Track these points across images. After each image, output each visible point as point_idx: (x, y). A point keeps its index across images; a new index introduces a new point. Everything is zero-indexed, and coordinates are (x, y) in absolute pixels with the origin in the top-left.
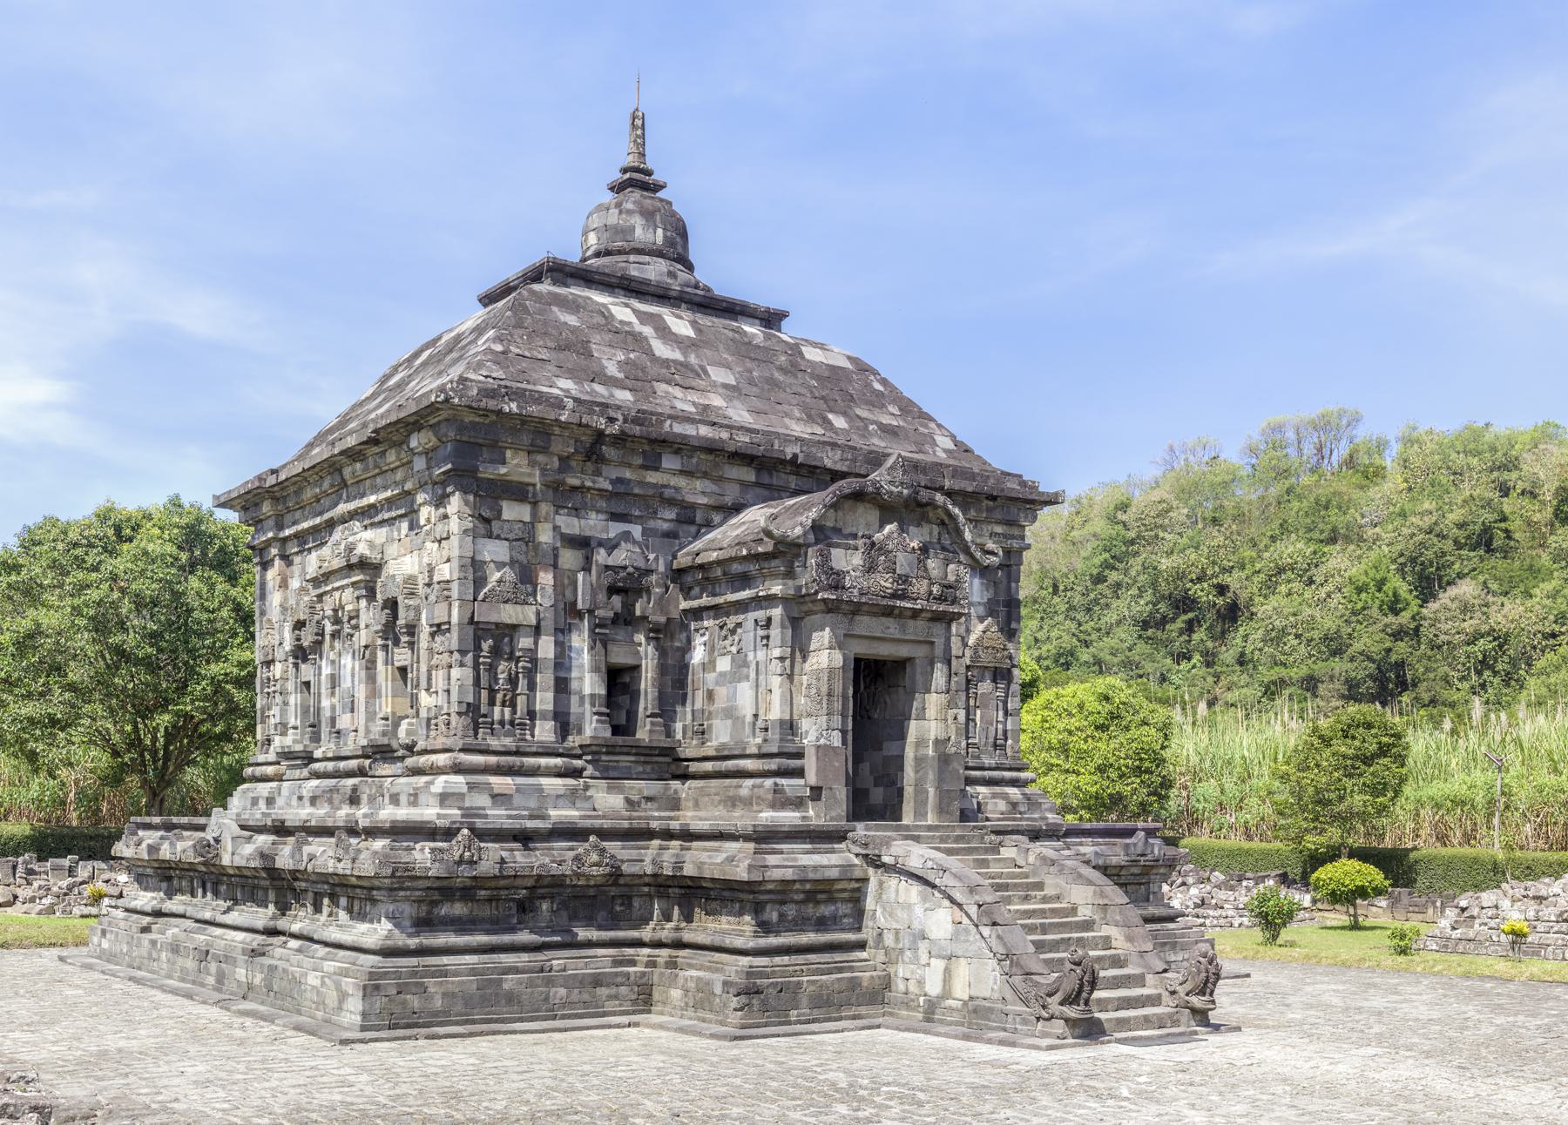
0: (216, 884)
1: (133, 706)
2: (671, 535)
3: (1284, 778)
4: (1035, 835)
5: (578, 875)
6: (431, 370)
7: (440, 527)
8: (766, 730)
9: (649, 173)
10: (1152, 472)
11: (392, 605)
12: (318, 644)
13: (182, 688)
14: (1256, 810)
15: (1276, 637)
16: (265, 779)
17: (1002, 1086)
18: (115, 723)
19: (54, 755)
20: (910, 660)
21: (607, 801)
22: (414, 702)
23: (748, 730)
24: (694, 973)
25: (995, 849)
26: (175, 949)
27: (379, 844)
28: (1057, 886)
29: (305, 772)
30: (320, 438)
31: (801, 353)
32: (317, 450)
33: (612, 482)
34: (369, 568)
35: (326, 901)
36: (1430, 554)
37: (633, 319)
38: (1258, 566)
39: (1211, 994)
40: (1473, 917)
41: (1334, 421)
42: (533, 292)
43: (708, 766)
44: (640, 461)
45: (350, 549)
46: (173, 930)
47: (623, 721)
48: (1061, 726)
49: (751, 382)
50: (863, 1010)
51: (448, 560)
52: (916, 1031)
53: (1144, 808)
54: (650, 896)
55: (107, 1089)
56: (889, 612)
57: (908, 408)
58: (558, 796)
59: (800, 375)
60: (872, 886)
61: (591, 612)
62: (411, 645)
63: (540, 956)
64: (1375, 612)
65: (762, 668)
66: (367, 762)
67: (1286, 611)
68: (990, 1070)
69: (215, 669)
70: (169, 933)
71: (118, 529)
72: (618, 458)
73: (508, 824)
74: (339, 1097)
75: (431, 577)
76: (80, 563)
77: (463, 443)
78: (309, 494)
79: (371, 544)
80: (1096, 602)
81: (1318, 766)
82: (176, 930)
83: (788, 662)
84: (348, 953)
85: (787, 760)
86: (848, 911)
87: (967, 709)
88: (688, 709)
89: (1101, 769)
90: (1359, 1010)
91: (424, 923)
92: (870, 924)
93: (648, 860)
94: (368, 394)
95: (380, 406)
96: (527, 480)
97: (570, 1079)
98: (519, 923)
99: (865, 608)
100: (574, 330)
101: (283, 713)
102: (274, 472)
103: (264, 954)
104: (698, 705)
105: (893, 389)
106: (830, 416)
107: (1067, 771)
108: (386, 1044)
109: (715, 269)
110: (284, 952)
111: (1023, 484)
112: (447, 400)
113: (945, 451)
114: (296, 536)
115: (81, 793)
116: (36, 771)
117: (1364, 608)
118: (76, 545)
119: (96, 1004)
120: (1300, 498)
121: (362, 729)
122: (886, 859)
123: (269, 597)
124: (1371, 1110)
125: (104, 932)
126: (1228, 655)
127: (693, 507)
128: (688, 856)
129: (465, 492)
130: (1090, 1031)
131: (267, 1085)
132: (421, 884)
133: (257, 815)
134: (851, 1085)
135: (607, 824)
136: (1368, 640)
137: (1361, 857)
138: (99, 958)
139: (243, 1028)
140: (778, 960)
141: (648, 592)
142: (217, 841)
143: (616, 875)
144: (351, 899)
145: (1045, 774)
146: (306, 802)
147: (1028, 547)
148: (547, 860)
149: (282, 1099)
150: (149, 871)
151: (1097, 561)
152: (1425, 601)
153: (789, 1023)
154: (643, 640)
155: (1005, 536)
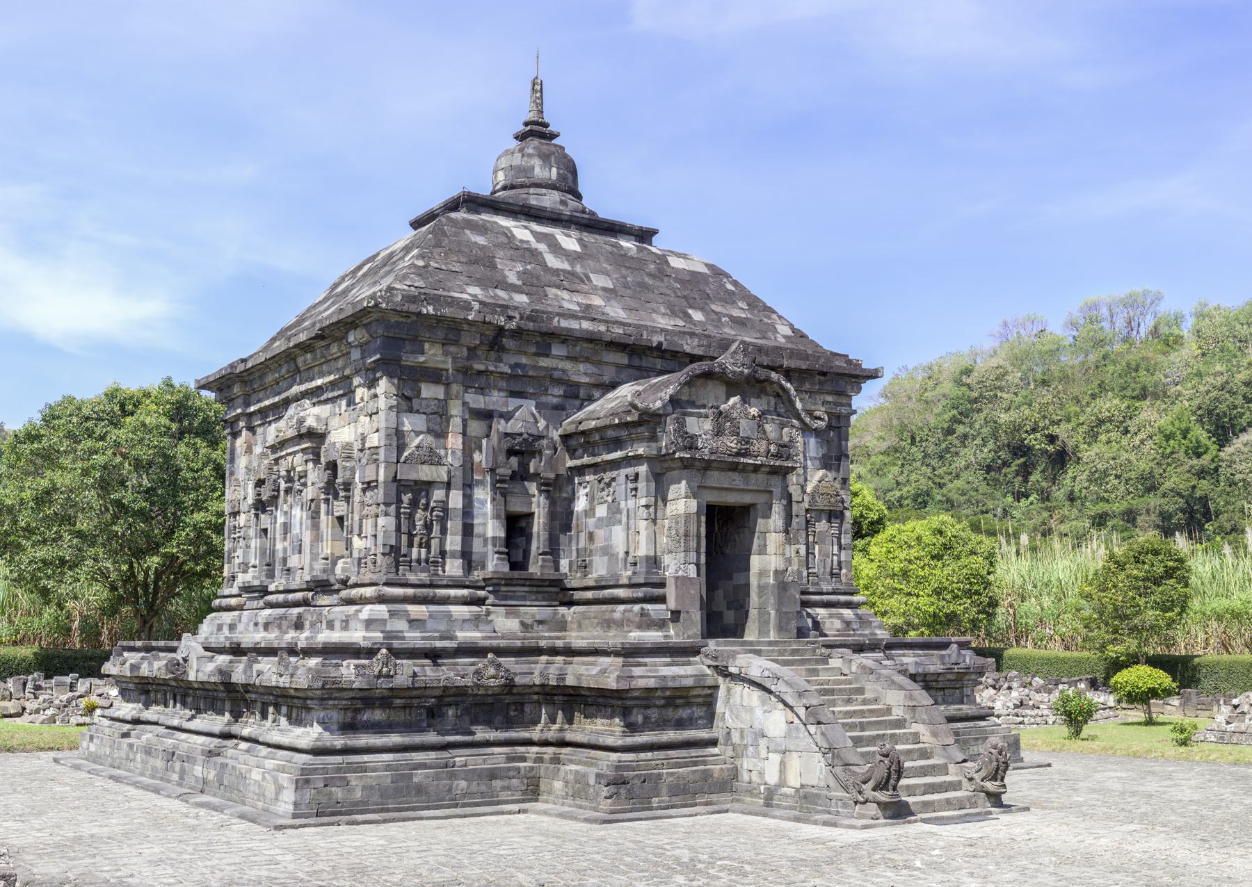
0: (184, 696)
1: (130, 549)
2: (559, 408)
3: (1088, 597)
4: (859, 648)
5: (478, 686)
6: (369, 280)
7: (371, 403)
8: (635, 564)
9: (546, 125)
10: (989, 344)
11: (332, 466)
12: (274, 499)
13: (169, 535)
14: (1069, 626)
15: (1098, 477)
16: (229, 609)
17: (817, 859)
18: (115, 562)
19: (64, 589)
20: (753, 505)
21: (505, 624)
22: (349, 544)
23: (621, 565)
24: (573, 767)
25: (825, 660)
26: (148, 751)
27: (313, 662)
28: (875, 690)
29: (261, 603)
30: (282, 333)
31: (667, 262)
32: (278, 343)
33: (511, 367)
34: (315, 437)
35: (271, 709)
36: (1222, 408)
37: (530, 238)
38: (1082, 419)
39: (1002, 780)
40: (1243, 713)
41: (1140, 300)
42: (450, 219)
43: (589, 595)
44: (533, 350)
45: (301, 422)
46: (147, 735)
47: (521, 559)
48: (902, 556)
49: (626, 286)
50: (714, 797)
51: (377, 431)
52: (756, 814)
53: (975, 624)
54: (539, 703)
55: (77, 867)
56: (734, 467)
57: (754, 303)
58: (464, 621)
59: (666, 279)
60: (722, 693)
61: (492, 470)
62: (347, 499)
63: (445, 754)
64: (1181, 455)
65: (632, 514)
66: (311, 594)
67: (1107, 456)
68: (811, 846)
69: (199, 517)
70: (144, 738)
71: (122, 406)
72: (511, 350)
73: (420, 644)
74: (265, 873)
75: (363, 444)
76: (90, 433)
77: (386, 338)
78: (270, 378)
79: (318, 418)
80: (947, 450)
81: (1115, 586)
82: (150, 735)
83: (652, 509)
84: (286, 752)
85: (651, 588)
86: (702, 714)
87: (807, 544)
88: (574, 548)
89: (937, 592)
90: (1134, 793)
91: (349, 727)
92: (721, 724)
93: (537, 673)
94: (321, 298)
95: (325, 310)
96: (441, 366)
97: (460, 857)
98: (429, 726)
99: (715, 465)
100: (482, 248)
101: (245, 554)
102: (244, 361)
103: (219, 755)
104: (582, 545)
105: (743, 288)
106: (690, 311)
107: (909, 594)
108: (313, 829)
109: (599, 198)
110: (236, 753)
111: (849, 362)
112: (376, 305)
113: (784, 337)
114: (260, 411)
115: (84, 619)
116: (48, 602)
117: (1173, 453)
118: (87, 419)
119: (79, 799)
120: (1114, 362)
121: (307, 568)
122: (732, 670)
123: (237, 461)
124: (1118, 876)
125: (92, 738)
126: (1059, 494)
127: (578, 385)
128: (570, 669)
129: (391, 376)
130: (898, 812)
131: (209, 863)
132: (346, 695)
133: (222, 639)
134: (692, 860)
135: (503, 643)
136: (1175, 479)
137: (1149, 661)
138: (87, 759)
139: (197, 817)
140: (642, 755)
141: (540, 453)
142: (185, 660)
143: (510, 686)
144: (290, 707)
145: (890, 597)
146: (261, 628)
147: (855, 412)
148: (452, 674)
149: (218, 875)
150: (131, 686)
151: (947, 417)
152: (1222, 446)
153: (651, 809)
154: (536, 492)
155: (835, 403)
